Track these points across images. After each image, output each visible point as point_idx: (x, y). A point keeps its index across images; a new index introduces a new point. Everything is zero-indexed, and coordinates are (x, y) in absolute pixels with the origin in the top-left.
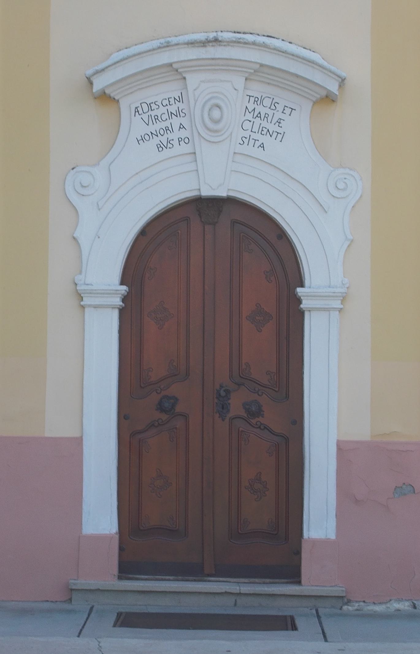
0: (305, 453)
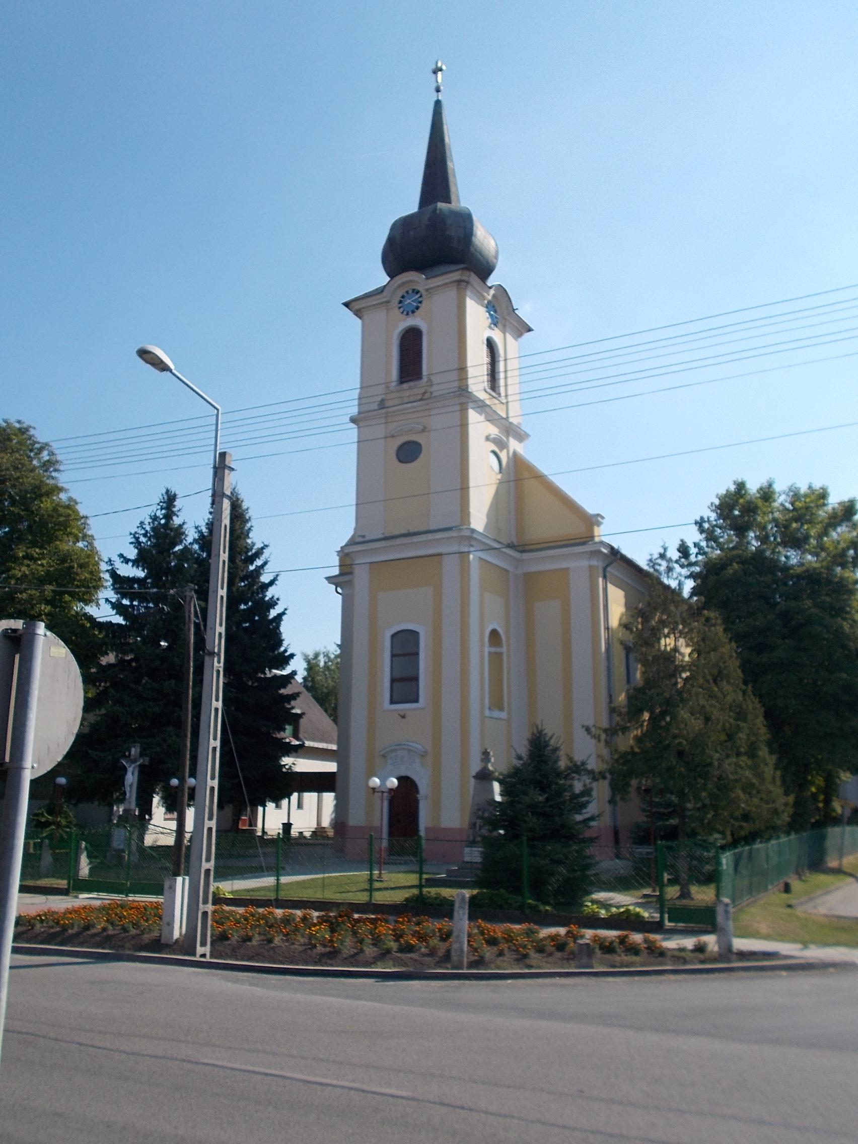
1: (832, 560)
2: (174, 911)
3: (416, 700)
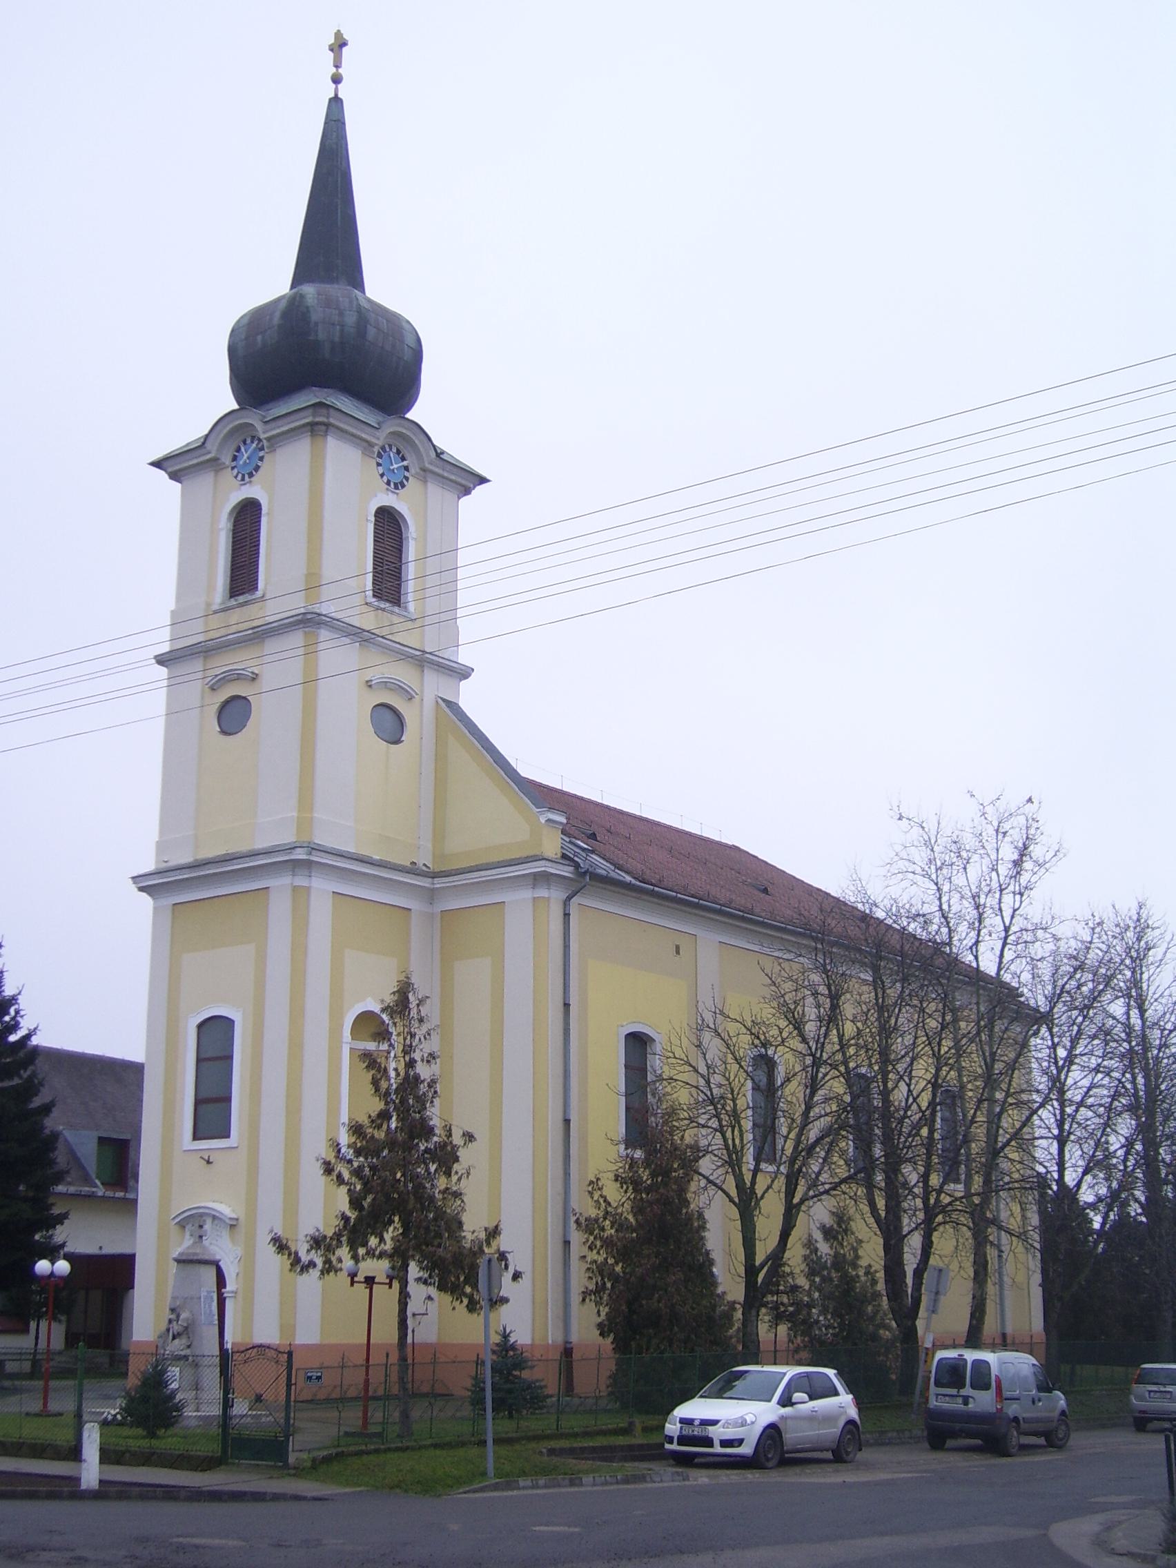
0: (227, 549)
1: (466, 1252)
2: (1044, 1326)
3: (227, 1135)
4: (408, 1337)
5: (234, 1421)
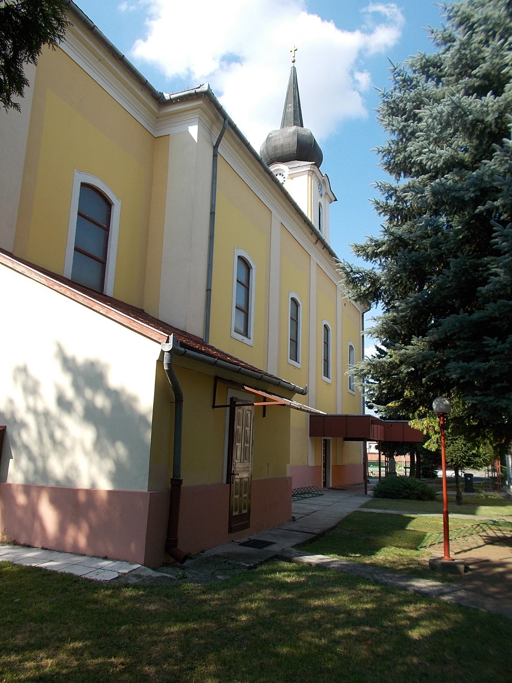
4: (475, 71)
5: (455, 102)
